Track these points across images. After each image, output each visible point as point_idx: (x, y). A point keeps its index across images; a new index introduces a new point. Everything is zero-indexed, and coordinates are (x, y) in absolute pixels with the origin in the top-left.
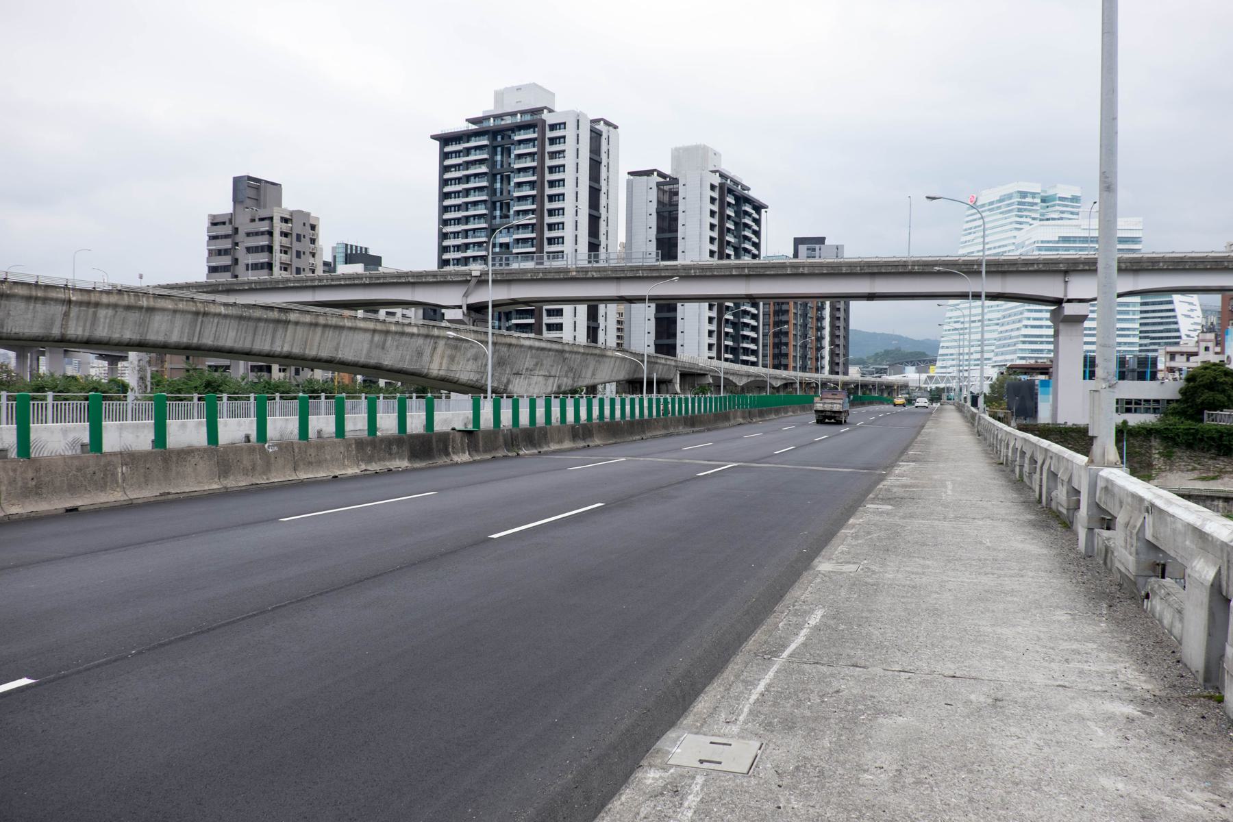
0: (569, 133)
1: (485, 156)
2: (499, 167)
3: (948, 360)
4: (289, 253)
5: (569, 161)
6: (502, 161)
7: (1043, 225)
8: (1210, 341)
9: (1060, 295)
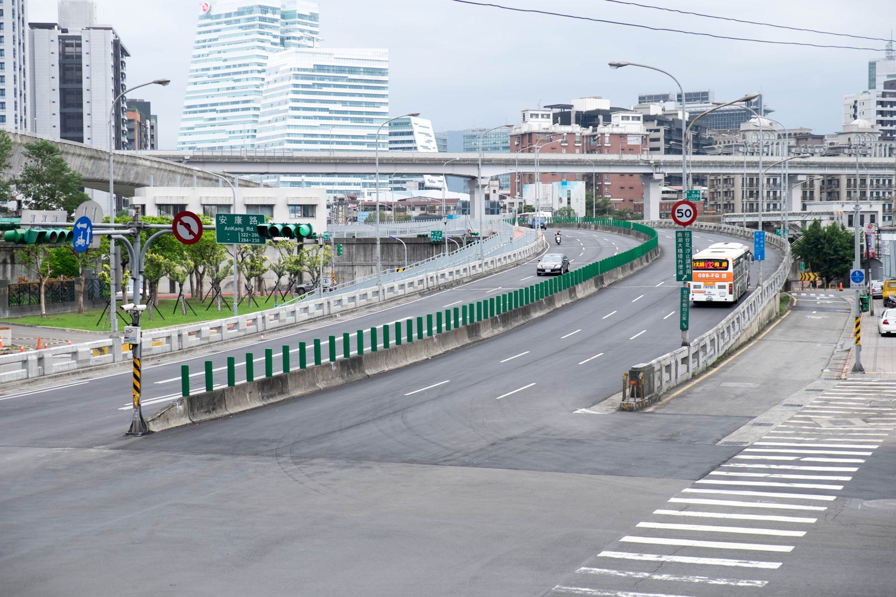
7: (298, 52)
8: (496, 186)
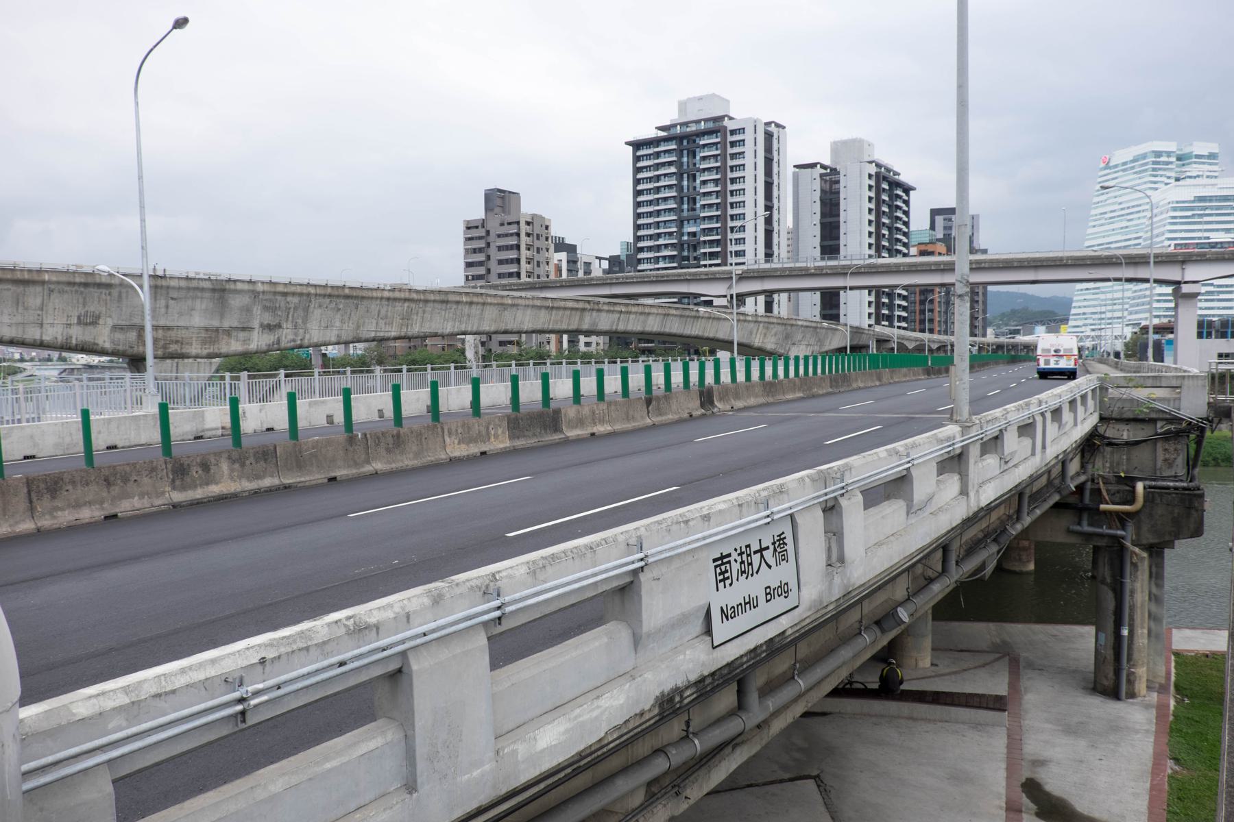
0: (748, 137)
1: (674, 159)
2: (685, 167)
3: (1081, 319)
4: (531, 249)
5: (748, 161)
6: (688, 162)
9: (1178, 278)
